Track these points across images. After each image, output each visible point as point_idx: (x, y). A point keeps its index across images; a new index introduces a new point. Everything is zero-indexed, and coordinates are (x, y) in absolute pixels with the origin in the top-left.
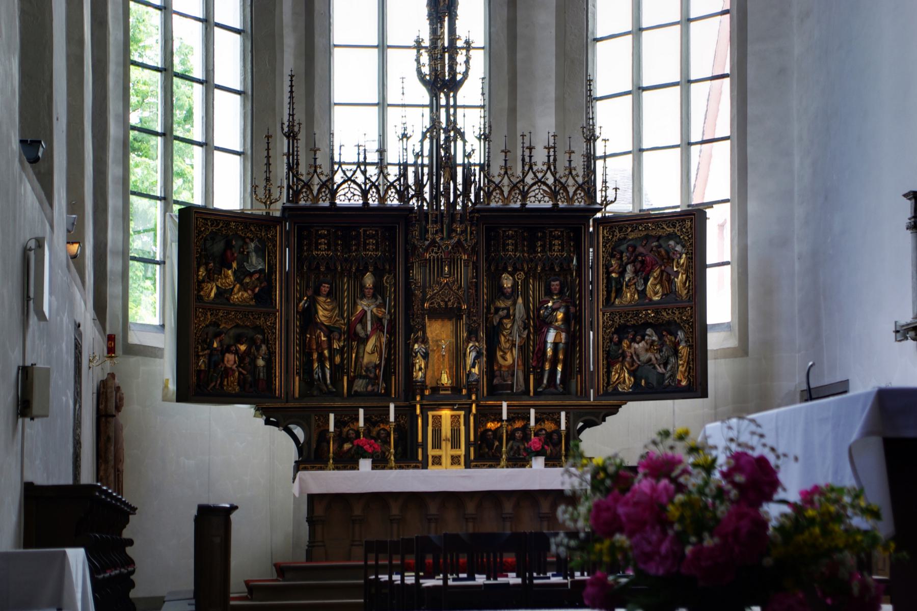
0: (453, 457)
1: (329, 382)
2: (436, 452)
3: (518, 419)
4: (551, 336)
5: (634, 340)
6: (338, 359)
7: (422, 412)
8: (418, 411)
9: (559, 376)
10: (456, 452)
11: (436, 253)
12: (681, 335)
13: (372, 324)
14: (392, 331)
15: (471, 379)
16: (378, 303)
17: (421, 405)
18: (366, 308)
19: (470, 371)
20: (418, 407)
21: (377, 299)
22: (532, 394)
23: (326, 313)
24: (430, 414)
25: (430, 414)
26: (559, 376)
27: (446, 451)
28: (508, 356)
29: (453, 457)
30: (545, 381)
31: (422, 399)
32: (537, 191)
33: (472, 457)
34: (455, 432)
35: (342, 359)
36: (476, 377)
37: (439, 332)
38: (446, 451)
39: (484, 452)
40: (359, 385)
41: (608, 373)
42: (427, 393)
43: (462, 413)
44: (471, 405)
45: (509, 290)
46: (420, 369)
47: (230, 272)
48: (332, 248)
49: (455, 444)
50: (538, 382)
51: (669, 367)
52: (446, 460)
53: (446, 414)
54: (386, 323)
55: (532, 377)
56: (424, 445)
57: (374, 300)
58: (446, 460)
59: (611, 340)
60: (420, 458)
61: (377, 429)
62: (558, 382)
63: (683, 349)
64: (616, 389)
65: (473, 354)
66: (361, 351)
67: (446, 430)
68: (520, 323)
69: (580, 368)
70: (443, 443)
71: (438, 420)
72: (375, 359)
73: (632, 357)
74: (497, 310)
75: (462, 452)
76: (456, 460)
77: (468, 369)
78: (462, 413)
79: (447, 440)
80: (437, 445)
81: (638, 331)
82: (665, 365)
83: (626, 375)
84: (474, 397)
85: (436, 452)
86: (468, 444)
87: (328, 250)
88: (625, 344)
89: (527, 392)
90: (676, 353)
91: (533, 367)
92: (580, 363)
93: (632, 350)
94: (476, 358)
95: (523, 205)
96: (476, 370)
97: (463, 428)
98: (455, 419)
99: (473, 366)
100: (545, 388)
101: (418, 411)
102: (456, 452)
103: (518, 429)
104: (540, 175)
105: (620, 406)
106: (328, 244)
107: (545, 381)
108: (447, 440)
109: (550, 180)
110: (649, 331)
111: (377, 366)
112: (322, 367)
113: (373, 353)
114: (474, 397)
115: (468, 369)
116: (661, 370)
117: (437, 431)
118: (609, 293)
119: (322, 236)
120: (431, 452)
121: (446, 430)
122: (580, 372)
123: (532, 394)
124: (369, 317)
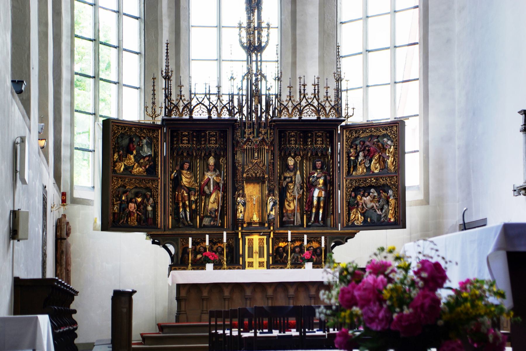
0: (260, 263)
1: (188, 219)
2: (250, 260)
3: (297, 240)
4: (316, 193)
5: (363, 195)
6: (194, 206)
7: (242, 237)
8: (240, 236)
9: (320, 216)
10: (261, 260)
11: (250, 145)
12: (390, 192)
13: (213, 186)
14: (225, 190)
15: (270, 218)
16: (217, 174)
17: (242, 233)
18: (210, 177)
19: (270, 213)
20: (240, 234)
21: (216, 172)
22: (305, 226)
23: (187, 180)
24: (247, 238)
25: (247, 238)
26: (320, 216)
27: (256, 260)
28: (292, 205)
29: (260, 263)
30: (313, 219)
31: (242, 229)
32: (308, 110)
33: (271, 263)
34: (261, 248)
35: (196, 206)
36: (273, 217)
37: (252, 191)
38: (256, 260)
39: (278, 260)
40: (206, 221)
41: (349, 214)
42: (245, 225)
43: (265, 237)
44: (270, 232)
45: (292, 167)
46: (241, 212)
47: (132, 156)
48: (191, 142)
49: (261, 255)
50: (309, 219)
51: (384, 211)
52: (256, 264)
53: (256, 238)
54: (221, 185)
55: (305, 216)
56: (243, 256)
57: (214, 172)
58: (256, 264)
59: (351, 195)
60: (241, 263)
61: (216, 246)
62: (320, 219)
63: (392, 201)
64: (353, 223)
65: (272, 203)
66: (207, 201)
67: (256, 248)
68: (298, 185)
69: (333, 211)
70: (254, 255)
71: (251, 241)
72: (215, 206)
73: (362, 205)
74: (285, 178)
75: (265, 259)
76: (261, 264)
77: (268, 212)
78: (265, 237)
79: (256, 253)
80: (251, 256)
81: (366, 190)
82: (382, 210)
83: (359, 215)
84: (272, 228)
85: (250, 260)
86: (269, 255)
87: (188, 143)
88: (359, 197)
89: (302, 225)
90: (388, 203)
91: (306, 211)
92: (333, 208)
93: (363, 201)
94: (273, 205)
95: (300, 118)
96: (273, 213)
97: (265, 246)
98: (261, 240)
99: (272, 210)
100: (313, 223)
101: (240, 236)
102: (261, 260)
103: (297, 247)
104: (310, 101)
105: (356, 233)
106: (188, 140)
107: (313, 219)
108: (256, 253)
109: (316, 104)
110: (372, 190)
111: (216, 211)
112: (185, 211)
113: (214, 203)
114: (272, 228)
115: (268, 212)
116: (379, 212)
117: (251, 248)
118: (349, 168)
119: (186, 136)
120: (247, 260)
121: (256, 248)
122: (333, 214)
123: (305, 226)
124: (212, 182)
